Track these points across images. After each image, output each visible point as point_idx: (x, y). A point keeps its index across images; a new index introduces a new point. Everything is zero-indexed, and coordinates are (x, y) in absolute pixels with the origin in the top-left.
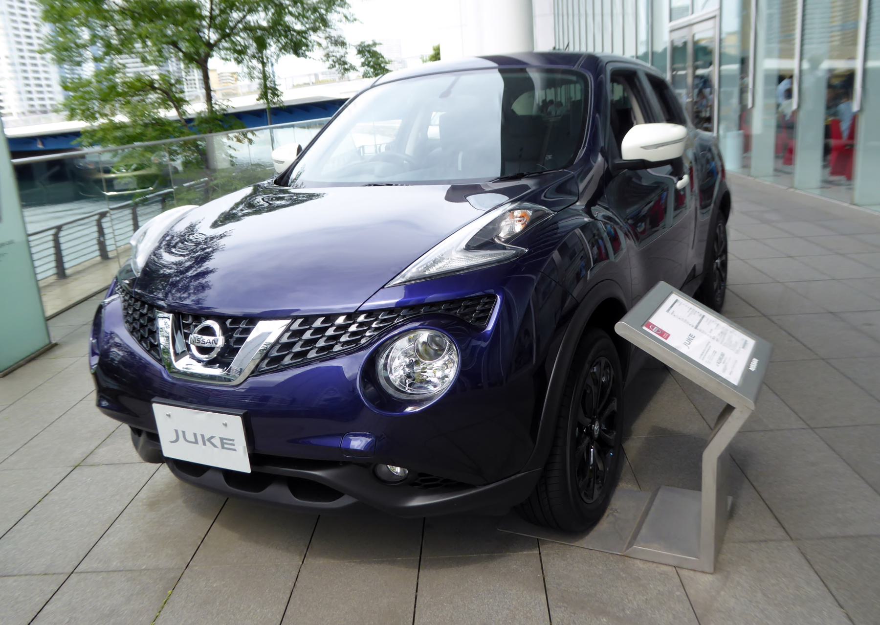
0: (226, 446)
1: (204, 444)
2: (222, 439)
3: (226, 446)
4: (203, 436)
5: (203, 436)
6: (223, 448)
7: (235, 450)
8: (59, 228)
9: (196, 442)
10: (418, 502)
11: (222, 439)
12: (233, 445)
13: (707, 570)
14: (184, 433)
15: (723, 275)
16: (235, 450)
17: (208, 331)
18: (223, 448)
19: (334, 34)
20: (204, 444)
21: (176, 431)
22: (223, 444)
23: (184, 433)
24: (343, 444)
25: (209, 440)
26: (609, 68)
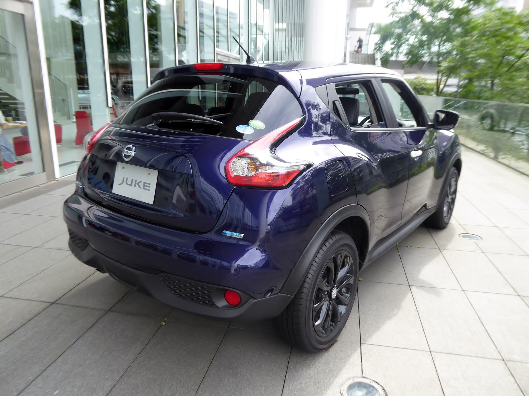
0: (145, 187)
1: (135, 186)
2: (145, 183)
3: (145, 187)
4: (136, 181)
6: (144, 188)
7: (149, 190)
8: (342, 64)
9: (131, 185)
10: (236, 235)
11: (145, 183)
13: (435, 353)
15: (452, 206)
16: (149, 190)
17: (129, 149)
18: (144, 188)
19: (484, 98)
20: (135, 186)
21: (124, 178)
22: (144, 186)
23: (127, 179)
24: (243, 153)
25: (138, 184)
26: (159, 33)
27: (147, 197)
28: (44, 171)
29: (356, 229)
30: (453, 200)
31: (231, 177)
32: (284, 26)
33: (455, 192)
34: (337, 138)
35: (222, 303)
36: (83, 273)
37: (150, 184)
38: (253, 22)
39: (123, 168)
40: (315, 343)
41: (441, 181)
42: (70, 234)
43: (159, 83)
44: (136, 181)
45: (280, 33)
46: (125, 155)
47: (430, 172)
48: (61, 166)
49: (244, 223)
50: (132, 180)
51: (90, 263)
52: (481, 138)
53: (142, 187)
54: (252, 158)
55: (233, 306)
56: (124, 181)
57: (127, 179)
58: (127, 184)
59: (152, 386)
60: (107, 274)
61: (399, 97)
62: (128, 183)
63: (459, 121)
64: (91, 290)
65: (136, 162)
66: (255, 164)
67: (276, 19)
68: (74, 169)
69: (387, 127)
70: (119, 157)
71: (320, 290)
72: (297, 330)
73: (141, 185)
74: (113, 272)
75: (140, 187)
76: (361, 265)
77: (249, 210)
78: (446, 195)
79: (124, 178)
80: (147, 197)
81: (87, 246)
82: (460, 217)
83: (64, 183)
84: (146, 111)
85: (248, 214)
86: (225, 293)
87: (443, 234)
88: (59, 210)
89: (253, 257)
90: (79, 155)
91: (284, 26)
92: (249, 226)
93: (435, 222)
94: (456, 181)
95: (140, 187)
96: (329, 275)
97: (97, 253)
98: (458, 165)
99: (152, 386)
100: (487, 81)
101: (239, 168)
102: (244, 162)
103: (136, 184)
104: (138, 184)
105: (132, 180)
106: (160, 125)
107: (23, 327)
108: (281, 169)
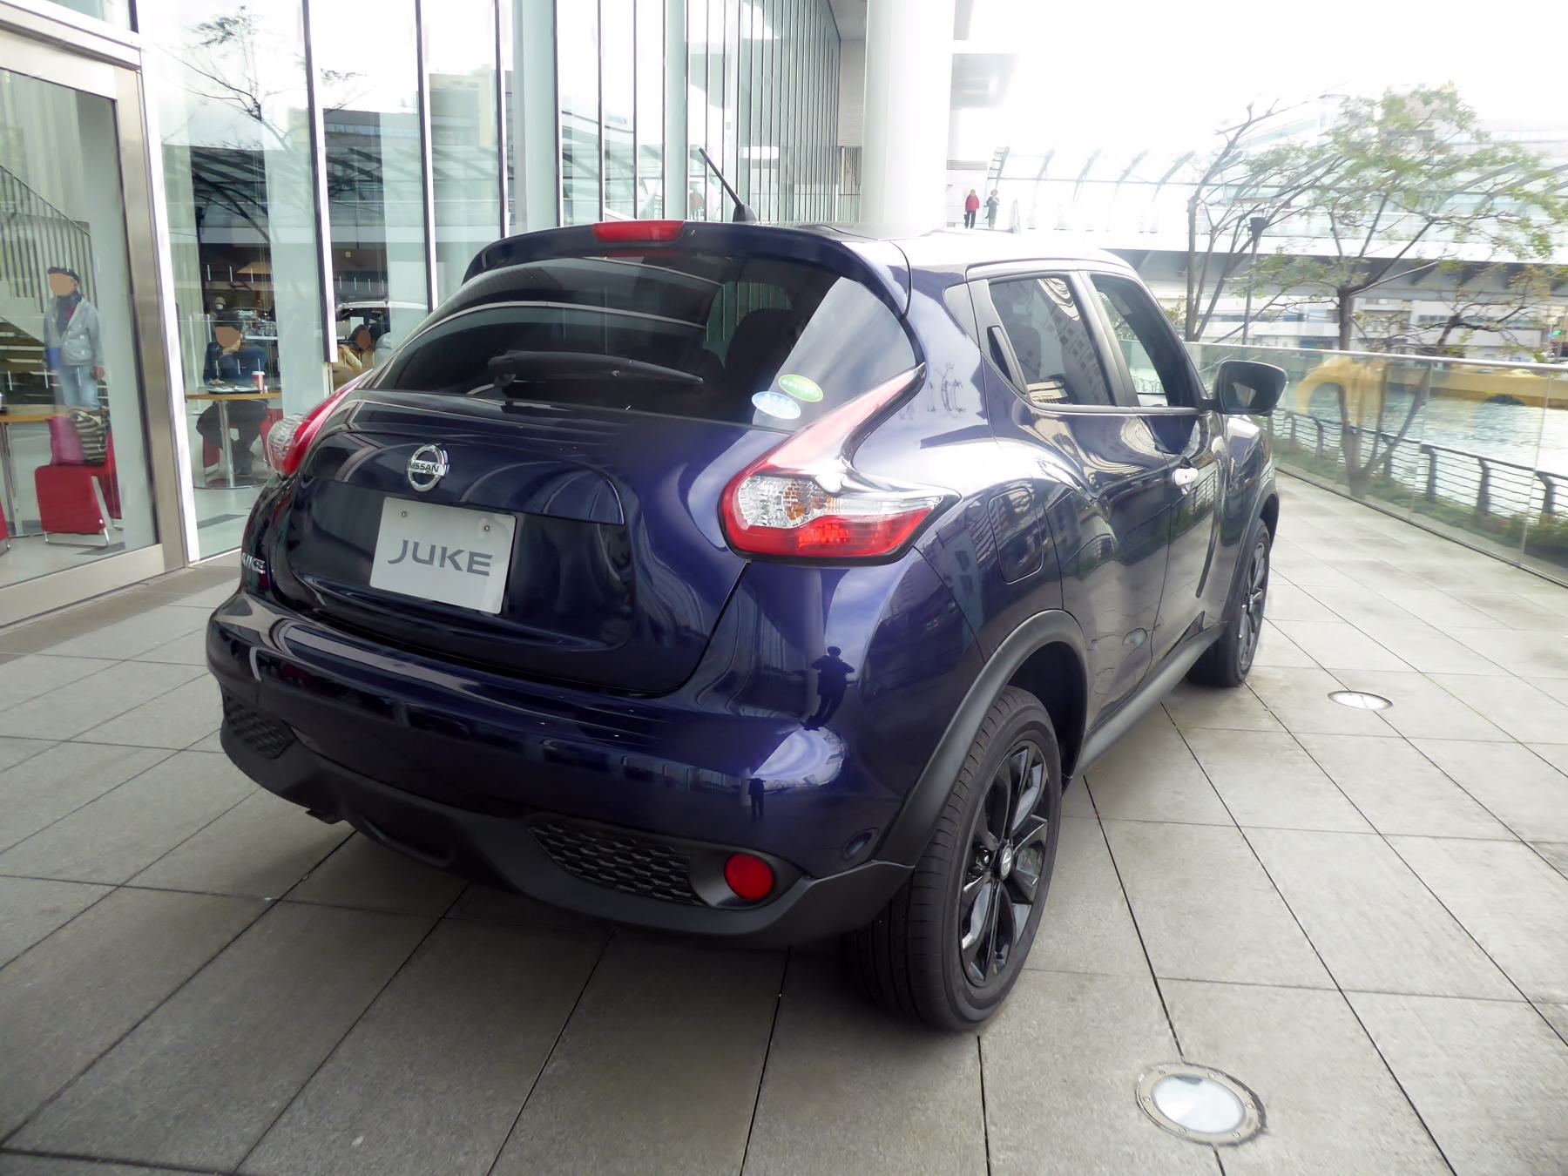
1: (442, 565)
2: (472, 555)
3: (475, 567)
4: (444, 550)
6: (470, 570)
7: (486, 574)
11: (472, 555)
18: (470, 570)
20: (442, 565)
21: (406, 543)
22: (471, 562)
23: (416, 545)
27: (485, 594)
28: (157, 541)
29: (1056, 679)
30: (1259, 604)
31: (738, 529)
32: (770, 153)
33: (1263, 584)
35: (717, 893)
36: (263, 821)
37: (489, 557)
38: (696, 140)
39: (404, 514)
40: (961, 1000)
41: (1234, 551)
42: (227, 712)
43: (496, 277)
44: (444, 550)
45: (765, 172)
46: (414, 475)
47: (1204, 533)
48: (200, 525)
49: (758, 660)
50: (433, 548)
51: (293, 794)
54: (796, 477)
55: (745, 901)
56: (409, 551)
57: (416, 545)
58: (415, 558)
59: (660, 1146)
60: (344, 826)
62: (420, 556)
64: (313, 862)
65: (440, 496)
66: (802, 487)
67: (746, 136)
68: (234, 535)
69: (1113, 403)
71: (978, 848)
72: (890, 965)
73: (463, 560)
74: (364, 814)
75: (457, 567)
76: (1065, 782)
77: (773, 622)
78: (1244, 591)
79: (406, 543)
80: (485, 594)
81: (289, 744)
82: (1274, 652)
83: (207, 577)
84: (447, 359)
85: (771, 636)
86: (726, 865)
87: (1242, 694)
88: (196, 648)
89: (803, 759)
90: (241, 503)
91: (770, 153)
92: (776, 669)
93: (1217, 669)
94: (1266, 557)
95: (457, 567)
96: (998, 803)
97: (325, 764)
98: (1270, 513)
99: (660, 1146)
101: (758, 505)
102: (770, 488)
103: (449, 559)
104: (452, 558)
105: (433, 548)
106: (510, 392)
107: (210, 967)
108: (873, 507)
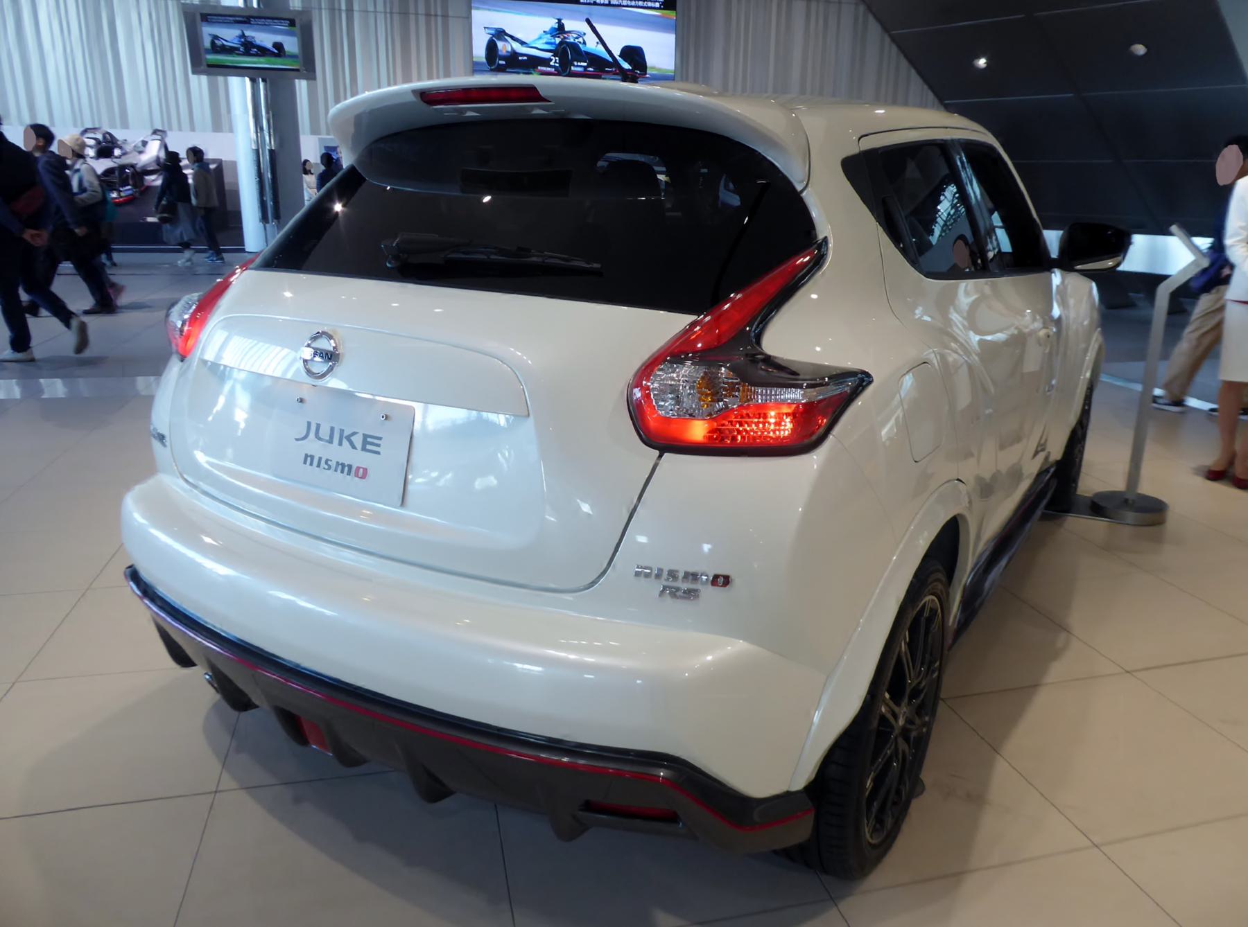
0: (369, 447)
1: (340, 444)
2: (365, 436)
3: (369, 447)
4: (342, 431)
5: (342, 431)
6: (364, 449)
7: (378, 453)
11: (365, 436)
12: (378, 445)
14: (318, 426)
16: (378, 453)
18: (364, 449)
20: (340, 444)
21: (309, 424)
22: (365, 443)
34: (964, 399)
37: (380, 439)
50: (332, 429)
52: (953, 344)
53: (359, 445)
61: (212, 691)
63: (151, 482)
70: (1045, 327)
75: (354, 447)
79: (309, 424)
95: (354, 447)
100: (774, 431)
104: (348, 438)
